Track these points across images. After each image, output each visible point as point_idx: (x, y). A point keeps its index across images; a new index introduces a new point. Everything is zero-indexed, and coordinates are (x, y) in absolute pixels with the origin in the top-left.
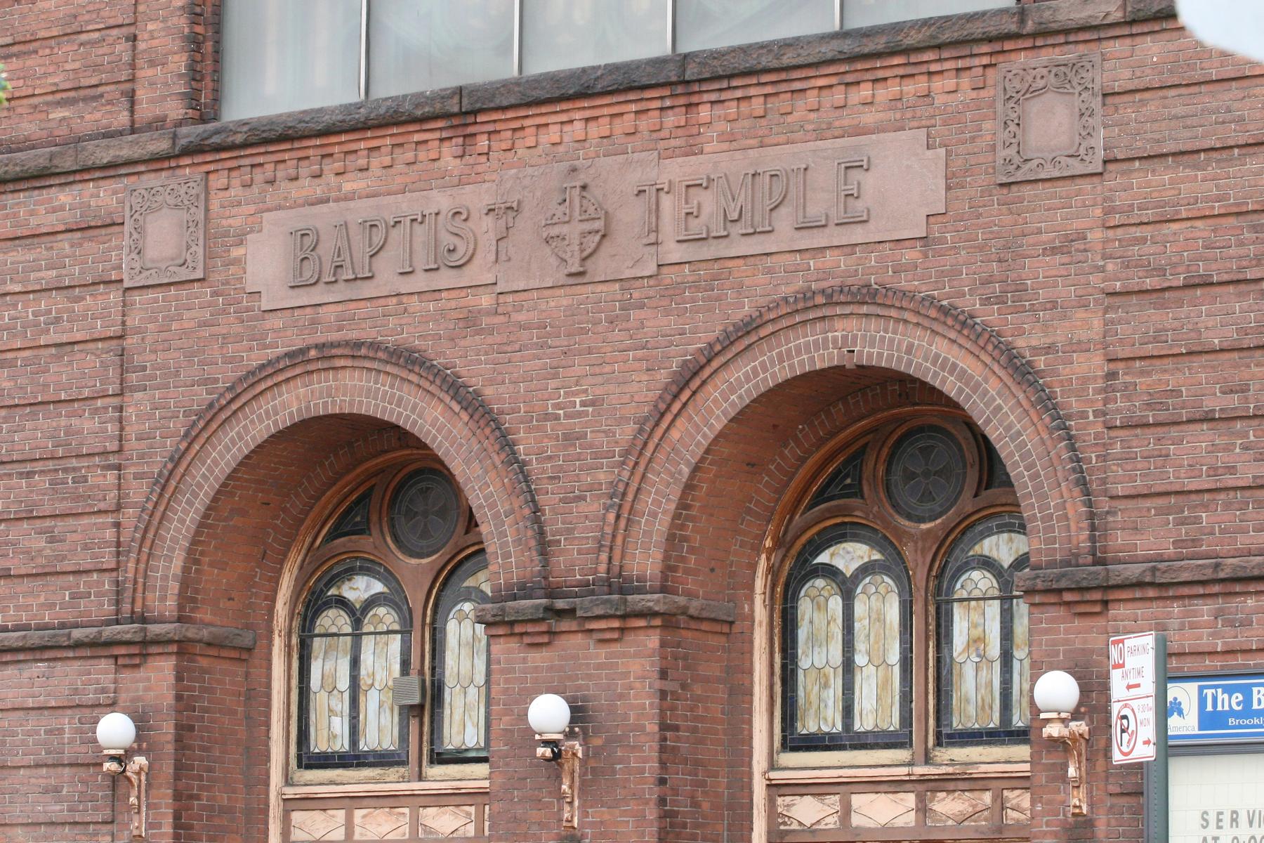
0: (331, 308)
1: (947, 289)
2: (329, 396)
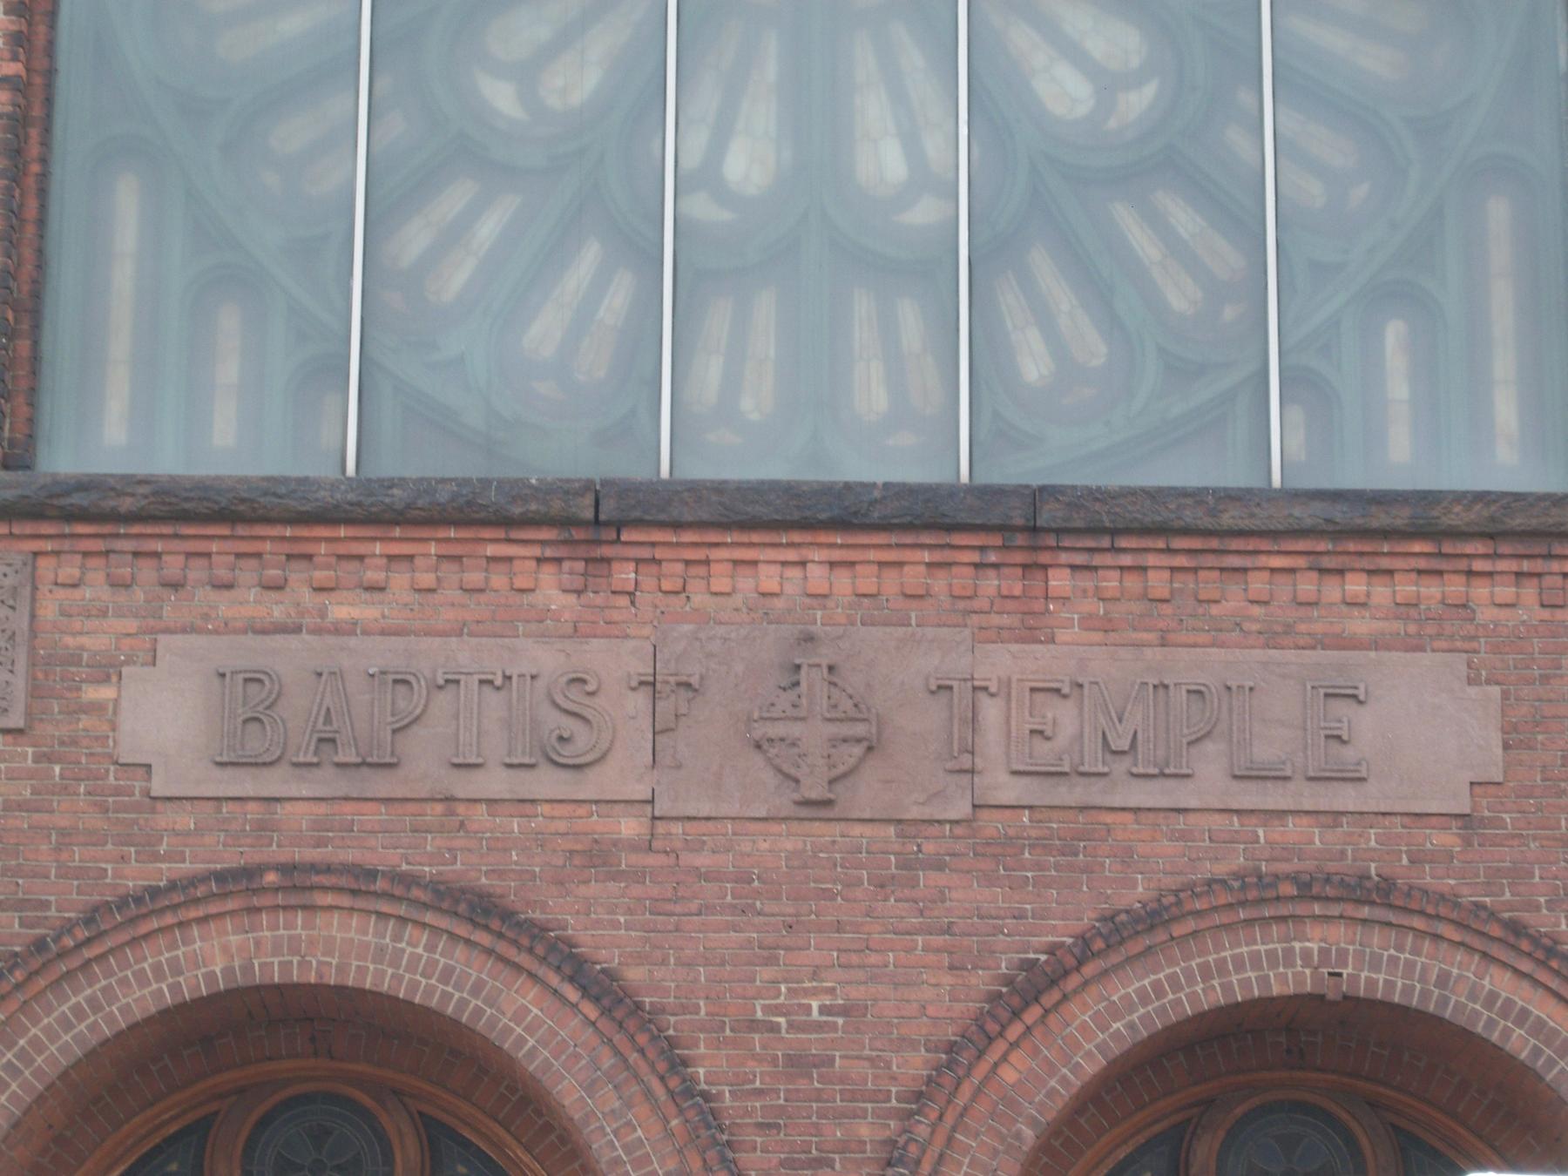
0: (301, 807)
1: (1508, 896)
2: (294, 951)
